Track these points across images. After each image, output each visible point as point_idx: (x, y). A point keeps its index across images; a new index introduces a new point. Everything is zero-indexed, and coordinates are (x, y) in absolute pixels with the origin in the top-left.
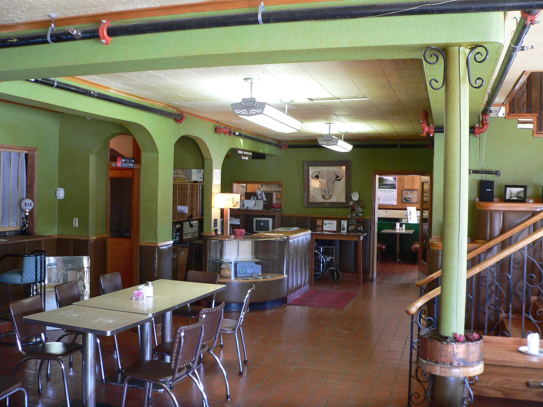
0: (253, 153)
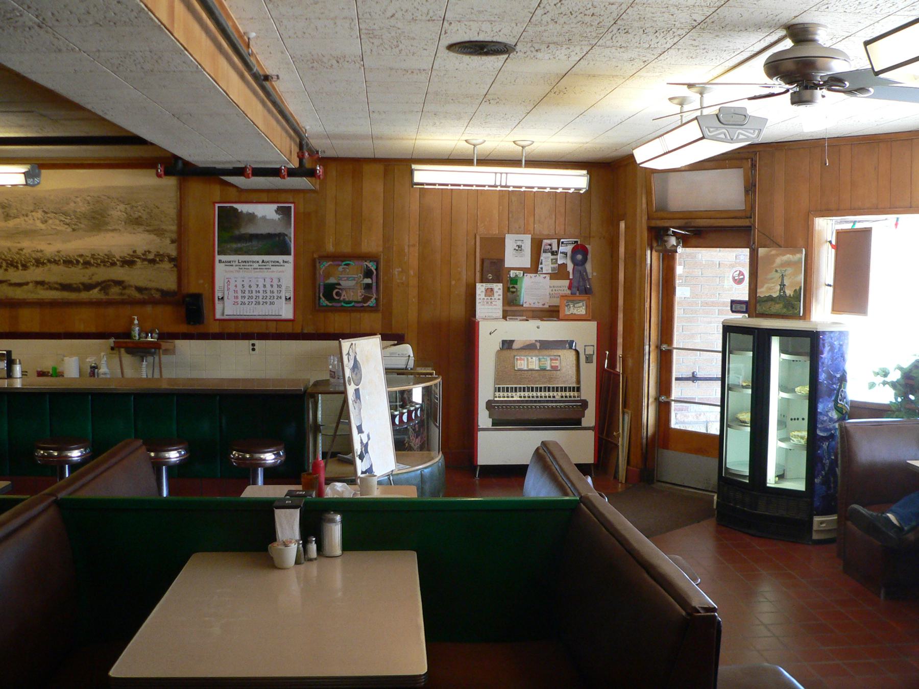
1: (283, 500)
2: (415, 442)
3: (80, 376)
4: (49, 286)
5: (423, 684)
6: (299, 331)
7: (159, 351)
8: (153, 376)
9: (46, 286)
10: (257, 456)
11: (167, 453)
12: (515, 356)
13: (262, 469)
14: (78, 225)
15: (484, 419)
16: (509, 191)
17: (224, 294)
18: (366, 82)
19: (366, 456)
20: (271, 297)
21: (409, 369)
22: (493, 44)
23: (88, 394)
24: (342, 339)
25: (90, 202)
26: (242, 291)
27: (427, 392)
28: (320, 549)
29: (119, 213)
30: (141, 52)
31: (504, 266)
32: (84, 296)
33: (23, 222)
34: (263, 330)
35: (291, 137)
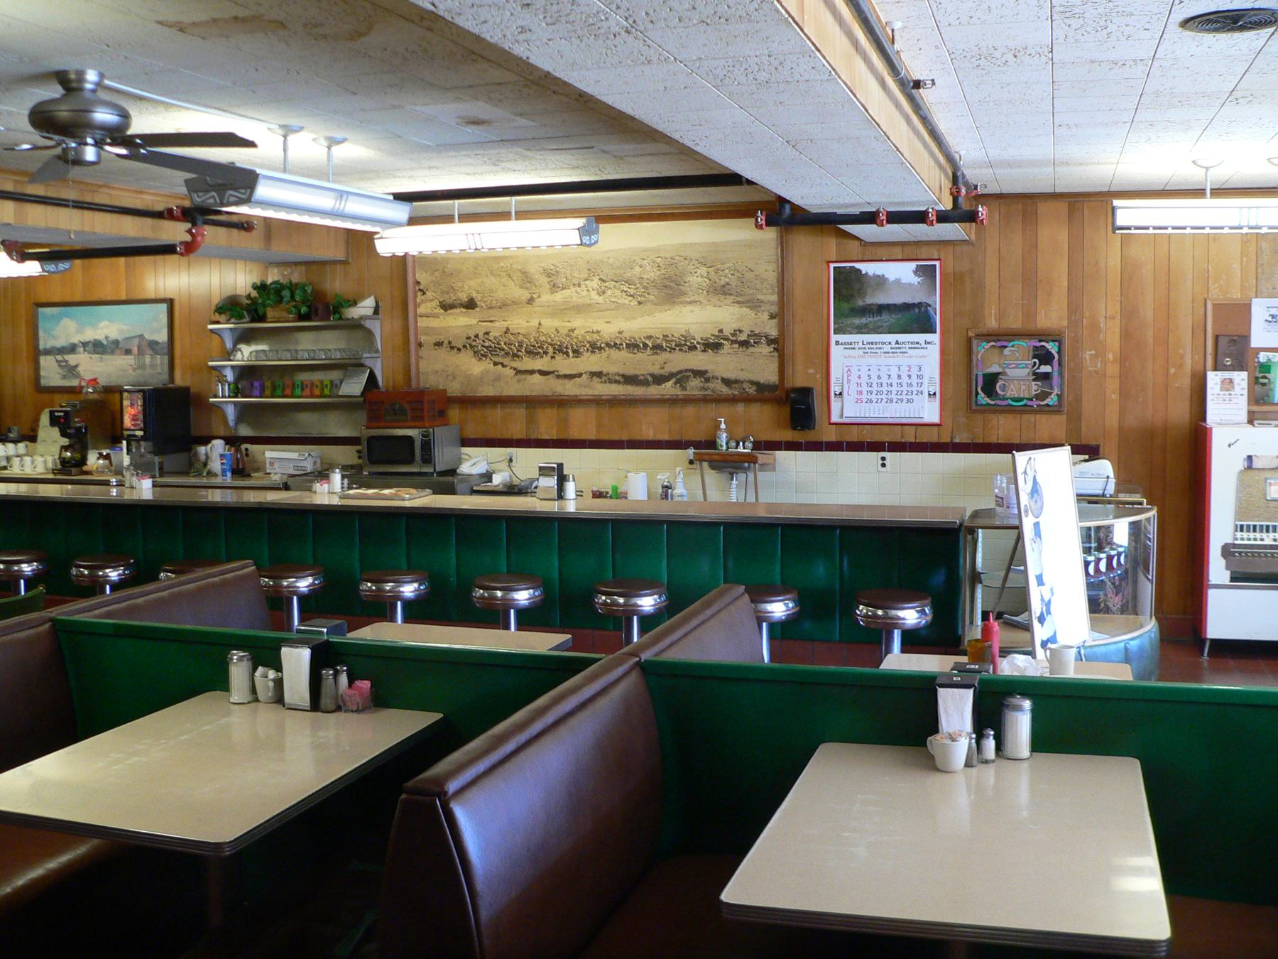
0: (109, 485)
1: (951, 676)
2: (1115, 601)
3: (648, 499)
4: (608, 379)
5: (1164, 954)
6: (948, 440)
7: (755, 467)
8: (745, 500)
9: (604, 378)
10: (893, 613)
11: (639, 599)
12: (1266, 479)
13: (900, 631)
14: (645, 297)
15: (1217, 570)
16: (1242, 234)
17: (843, 388)
18: (1053, 82)
19: (1048, 618)
20: (898, 391)
21: (1108, 496)
22: (1252, 13)
23: (664, 522)
24: (1017, 451)
25: (661, 265)
26: (868, 384)
27: (1135, 529)
28: (999, 747)
29: (700, 279)
30: (756, 56)
31: (1250, 345)
32: (654, 391)
33: (574, 294)
34: (897, 438)
35: (940, 167)
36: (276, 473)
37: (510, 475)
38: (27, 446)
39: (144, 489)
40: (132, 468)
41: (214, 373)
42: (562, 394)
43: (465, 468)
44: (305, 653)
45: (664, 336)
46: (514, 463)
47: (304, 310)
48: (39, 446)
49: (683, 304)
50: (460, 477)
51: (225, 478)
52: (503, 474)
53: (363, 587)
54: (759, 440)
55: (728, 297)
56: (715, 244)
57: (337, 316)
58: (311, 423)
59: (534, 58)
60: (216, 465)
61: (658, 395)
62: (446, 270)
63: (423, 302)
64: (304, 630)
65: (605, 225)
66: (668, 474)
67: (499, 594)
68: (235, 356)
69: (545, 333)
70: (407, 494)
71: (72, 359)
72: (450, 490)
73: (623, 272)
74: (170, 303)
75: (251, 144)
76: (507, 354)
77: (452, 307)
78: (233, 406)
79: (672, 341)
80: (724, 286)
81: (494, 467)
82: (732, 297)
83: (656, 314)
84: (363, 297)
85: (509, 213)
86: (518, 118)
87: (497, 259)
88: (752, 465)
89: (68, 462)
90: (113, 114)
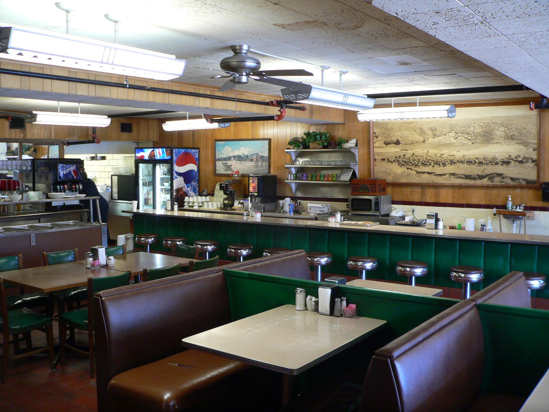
0: (243, 215)
9: (456, 176)
25: (483, 126)
29: (501, 133)
32: (479, 182)
36: (312, 213)
37: (413, 218)
38: (210, 198)
39: (258, 217)
40: (253, 208)
41: (287, 170)
42: (437, 183)
43: (393, 214)
44: (329, 291)
45: (484, 158)
46: (415, 212)
47: (325, 144)
48: (215, 198)
49: (493, 143)
50: (391, 217)
51: (290, 214)
52: (409, 217)
53: (349, 263)
54: (527, 206)
55: (514, 141)
56: (508, 117)
57: (340, 147)
58: (326, 192)
59: (438, 35)
60: (287, 208)
61: (480, 184)
62: (387, 127)
63: (377, 141)
64: (328, 281)
65: (458, 108)
66: (484, 220)
67: (408, 269)
68: (296, 163)
69: (430, 156)
70: (369, 224)
71: (229, 163)
72: (387, 223)
73: (465, 129)
74: (270, 140)
75: (311, 74)
76: (413, 164)
77: (389, 143)
78: (295, 184)
79: (487, 160)
80: (512, 136)
81: (406, 213)
82: (515, 141)
83: (480, 148)
84: (351, 139)
85: (416, 103)
86: (423, 62)
87: (410, 123)
88: (523, 217)
89: (226, 205)
90: (254, 63)
